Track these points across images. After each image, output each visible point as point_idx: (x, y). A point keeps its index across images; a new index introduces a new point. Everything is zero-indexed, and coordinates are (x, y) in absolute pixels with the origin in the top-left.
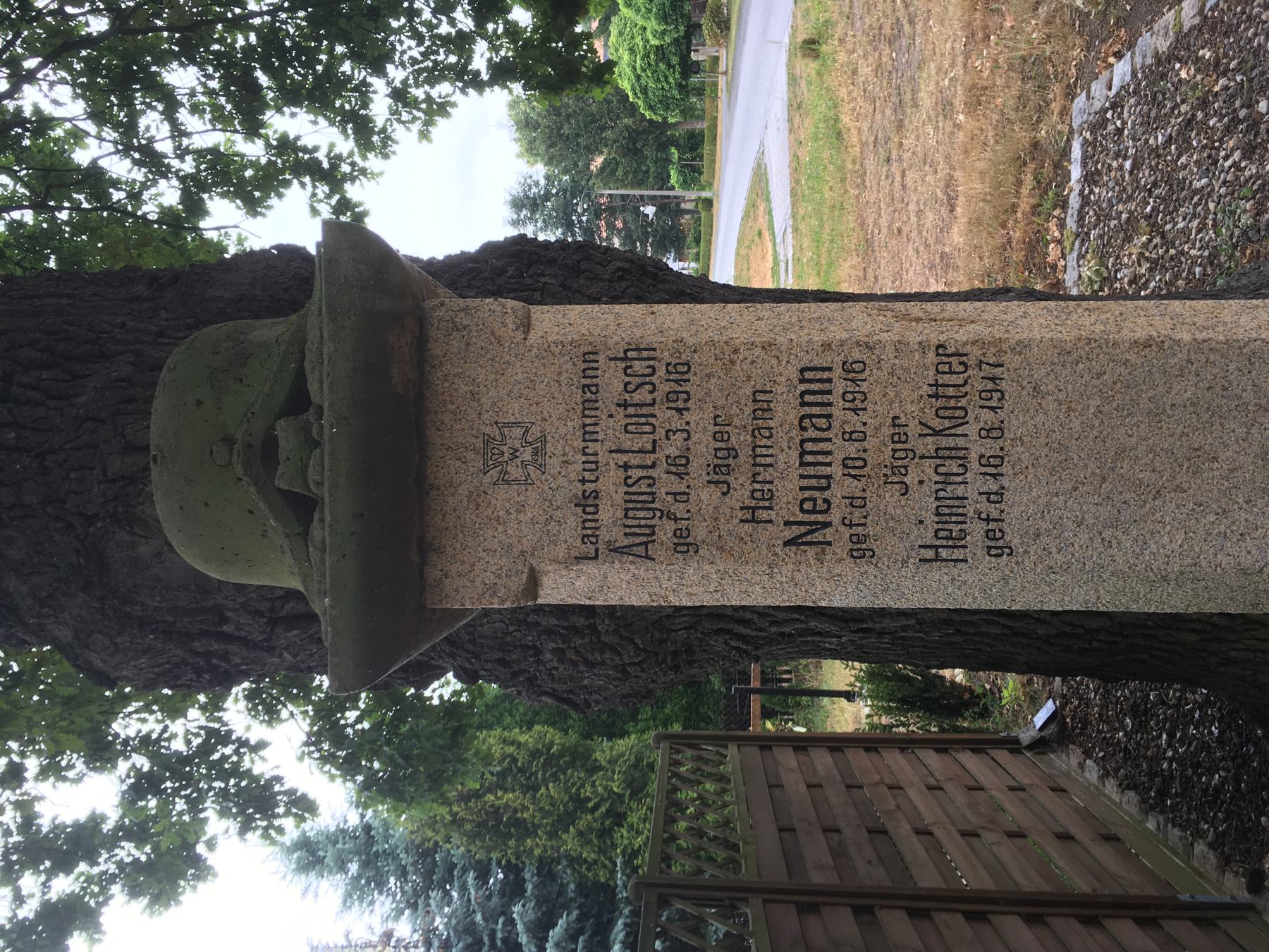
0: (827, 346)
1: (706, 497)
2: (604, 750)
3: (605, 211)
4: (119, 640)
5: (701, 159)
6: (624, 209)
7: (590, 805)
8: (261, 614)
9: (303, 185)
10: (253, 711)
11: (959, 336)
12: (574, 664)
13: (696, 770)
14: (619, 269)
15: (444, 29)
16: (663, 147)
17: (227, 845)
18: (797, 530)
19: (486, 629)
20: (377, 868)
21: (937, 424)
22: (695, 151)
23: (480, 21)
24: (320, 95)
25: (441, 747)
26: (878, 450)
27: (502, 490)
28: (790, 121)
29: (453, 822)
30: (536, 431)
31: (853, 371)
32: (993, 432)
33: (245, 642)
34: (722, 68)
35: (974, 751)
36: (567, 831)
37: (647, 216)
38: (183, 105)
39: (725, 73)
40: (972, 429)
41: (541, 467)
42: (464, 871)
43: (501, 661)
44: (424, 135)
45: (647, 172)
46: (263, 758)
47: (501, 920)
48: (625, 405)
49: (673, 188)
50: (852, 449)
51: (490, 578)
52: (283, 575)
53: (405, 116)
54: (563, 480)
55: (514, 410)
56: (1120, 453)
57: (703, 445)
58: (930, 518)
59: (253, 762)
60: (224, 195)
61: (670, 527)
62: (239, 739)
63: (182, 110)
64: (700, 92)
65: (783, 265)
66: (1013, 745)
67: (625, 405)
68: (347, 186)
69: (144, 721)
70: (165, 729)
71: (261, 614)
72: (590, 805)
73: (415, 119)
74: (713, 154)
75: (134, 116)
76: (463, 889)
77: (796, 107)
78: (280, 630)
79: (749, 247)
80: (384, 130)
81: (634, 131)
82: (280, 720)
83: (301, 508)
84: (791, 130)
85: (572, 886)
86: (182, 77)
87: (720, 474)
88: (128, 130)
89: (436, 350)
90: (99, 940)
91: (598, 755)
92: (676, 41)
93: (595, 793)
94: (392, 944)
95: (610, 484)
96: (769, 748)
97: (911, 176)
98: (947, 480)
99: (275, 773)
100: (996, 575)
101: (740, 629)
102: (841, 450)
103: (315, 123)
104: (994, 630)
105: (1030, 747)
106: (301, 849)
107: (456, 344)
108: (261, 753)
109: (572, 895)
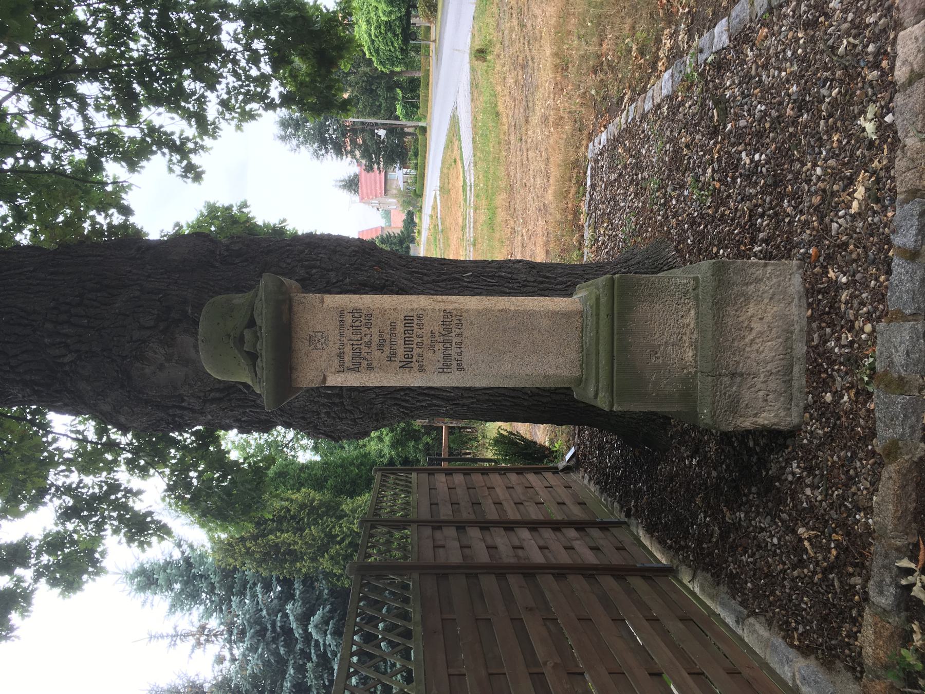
0: (412, 310)
1: (377, 354)
2: (347, 505)
3: (349, 131)
4: (135, 409)
5: (418, 99)
6: (363, 130)
7: (338, 539)
8: (200, 398)
9: (164, 154)
10: (131, 470)
11: (450, 307)
12: (334, 418)
13: (395, 483)
14: (354, 251)
15: (254, 72)
16: (390, 89)
17: (118, 553)
18: (403, 364)
19: (297, 404)
20: (194, 585)
21: (444, 333)
22: (414, 91)
23: (275, 68)
24: (173, 99)
25: (250, 490)
26: (427, 340)
27: (315, 352)
28: (472, 93)
29: (247, 553)
30: (325, 334)
31: (419, 317)
32: (459, 335)
33: (193, 411)
34: (432, 37)
35: (535, 473)
36: (323, 557)
37: (380, 136)
38: (90, 105)
39: (434, 41)
40: (453, 334)
41: (327, 345)
42: (255, 584)
43: (303, 418)
44: (239, 128)
45: (380, 106)
46: (140, 500)
47: (279, 615)
48: (352, 326)
49: (397, 118)
50: (419, 340)
51: (311, 378)
52: (244, 377)
53: (227, 116)
54: (333, 348)
55: (319, 328)
56: (495, 341)
57: (376, 339)
58: (441, 360)
59: (134, 502)
60: (116, 159)
61: (366, 362)
62: (126, 488)
63: (90, 108)
64: (417, 49)
65: (468, 188)
66: (555, 470)
67: (352, 326)
68: (192, 156)
69: (67, 476)
70: (81, 481)
71: (200, 398)
72: (338, 539)
73: (233, 118)
74: (427, 96)
75: (57, 109)
76: (254, 596)
77: (474, 85)
78: (207, 405)
79: (449, 169)
80: (214, 123)
81: (370, 76)
82: (149, 476)
83: (253, 357)
84: (472, 100)
85: (326, 591)
86: (89, 89)
87: (381, 347)
88: (54, 118)
89: (295, 309)
90: (28, 616)
91: (344, 507)
92: (400, 19)
93: (342, 532)
94: (206, 633)
95: (348, 349)
96: (433, 474)
97: (531, 154)
98: (446, 349)
99: (150, 509)
100: (460, 377)
101: (404, 404)
102: (416, 340)
103: (173, 118)
104: (508, 404)
105: (562, 470)
106: (140, 575)
107: (301, 307)
108: (140, 497)
109: (326, 596)
